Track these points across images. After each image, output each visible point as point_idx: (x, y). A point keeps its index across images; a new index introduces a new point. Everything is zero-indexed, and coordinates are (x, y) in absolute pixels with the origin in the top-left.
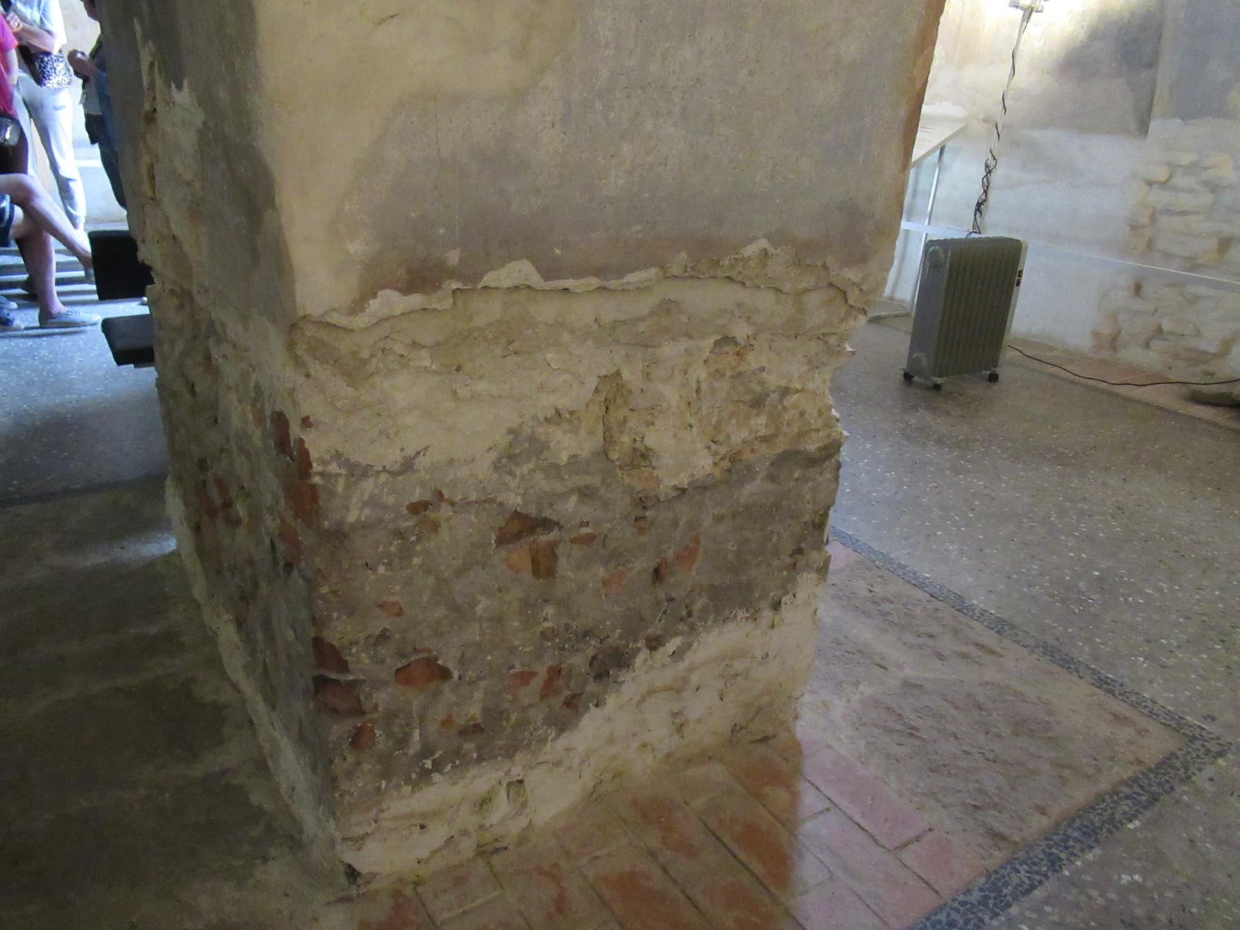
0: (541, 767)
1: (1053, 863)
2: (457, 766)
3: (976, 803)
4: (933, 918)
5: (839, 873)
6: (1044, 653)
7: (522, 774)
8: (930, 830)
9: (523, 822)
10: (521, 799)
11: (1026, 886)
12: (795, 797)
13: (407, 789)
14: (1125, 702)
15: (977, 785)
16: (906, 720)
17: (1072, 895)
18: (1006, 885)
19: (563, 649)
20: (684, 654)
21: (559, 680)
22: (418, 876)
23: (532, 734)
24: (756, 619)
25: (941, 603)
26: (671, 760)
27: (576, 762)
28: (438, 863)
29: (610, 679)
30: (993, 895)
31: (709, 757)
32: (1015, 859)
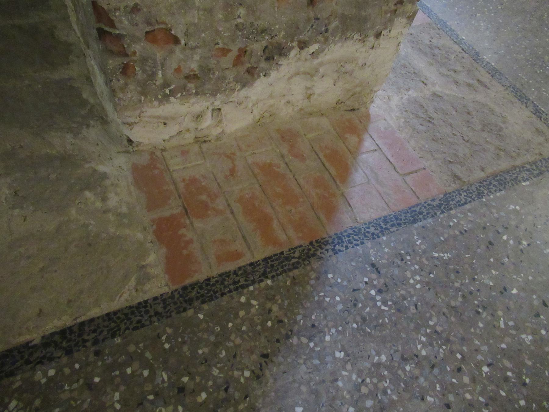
0: (231, 103)
1: (479, 194)
2: (184, 95)
3: (451, 160)
4: (413, 209)
5: (373, 181)
6: (512, 91)
7: (220, 106)
8: (424, 169)
9: (219, 130)
10: (219, 119)
11: (462, 202)
12: (361, 141)
13: (156, 103)
14: (545, 124)
15: (454, 152)
16: (429, 113)
17: (484, 210)
18: (453, 200)
19: (248, 38)
20: (318, 54)
21: (244, 57)
22: (164, 147)
23: (227, 85)
24: (364, 42)
25: (467, 55)
26: (302, 112)
27: (250, 105)
28: (174, 142)
29: (275, 62)
30: (445, 203)
31: (322, 114)
32: (461, 189)
